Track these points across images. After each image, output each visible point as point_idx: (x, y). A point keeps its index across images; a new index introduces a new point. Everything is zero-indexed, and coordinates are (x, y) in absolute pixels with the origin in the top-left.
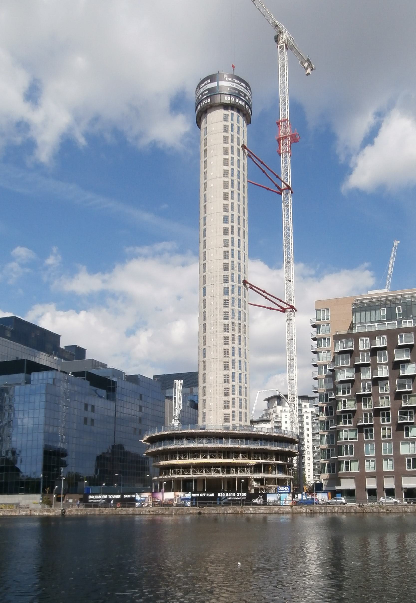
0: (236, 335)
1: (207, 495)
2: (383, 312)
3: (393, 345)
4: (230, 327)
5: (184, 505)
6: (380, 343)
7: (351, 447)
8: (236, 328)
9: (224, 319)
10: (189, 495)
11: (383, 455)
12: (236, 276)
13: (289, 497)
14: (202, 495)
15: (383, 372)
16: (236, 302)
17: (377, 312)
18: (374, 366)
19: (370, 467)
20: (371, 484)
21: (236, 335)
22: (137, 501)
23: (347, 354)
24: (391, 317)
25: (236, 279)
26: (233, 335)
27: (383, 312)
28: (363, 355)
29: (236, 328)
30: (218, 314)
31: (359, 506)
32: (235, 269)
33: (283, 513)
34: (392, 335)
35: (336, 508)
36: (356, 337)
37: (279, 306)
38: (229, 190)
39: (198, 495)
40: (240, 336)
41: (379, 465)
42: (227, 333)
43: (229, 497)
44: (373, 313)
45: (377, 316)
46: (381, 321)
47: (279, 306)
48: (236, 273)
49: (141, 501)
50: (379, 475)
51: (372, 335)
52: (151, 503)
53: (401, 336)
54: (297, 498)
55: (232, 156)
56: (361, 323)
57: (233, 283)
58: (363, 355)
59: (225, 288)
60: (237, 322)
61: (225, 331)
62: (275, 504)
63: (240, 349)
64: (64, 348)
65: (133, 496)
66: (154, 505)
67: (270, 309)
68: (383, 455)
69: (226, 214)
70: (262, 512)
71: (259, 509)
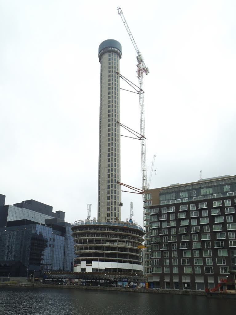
0: (113, 207)
1: (92, 280)
2: (174, 195)
3: (177, 212)
4: (110, 203)
5: (83, 285)
6: (172, 210)
7: (158, 261)
8: (113, 203)
9: (108, 200)
10: (84, 281)
11: (173, 265)
12: (114, 180)
13: (127, 284)
14: (90, 281)
15: (173, 224)
16: (113, 192)
17: (171, 195)
18: (168, 221)
19: (167, 270)
20: (167, 280)
21: (113, 207)
22: (64, 282)
23: (218, 209)
24: (178, 197)
25: (114, 181)
26: (112, 207)
27: (174, 195)
28: (192, 213)
29: (113, 203)
30: (105, 197)
31: (157, 290)
32: (113, 177)
33: (176, 294)
34: (177, 206)
35: (146, 290)
36: (160, 207)
37: (139, 192)
38: (111, 142)
39: (88, 280)
40: (115, 207)
41: (171, 270)
42: (109, 206)
43: (101, 282)
44: (169, 195)
45: (171, 196)
46: (173, 199)
47: (139, 192)
48: (114, 179)
49: (65, 282)
50: (171, 275)
51: (168, 206)
52: (69, 283)
53: (182, 207)
54: (131, 284)
55: (112, 127)
56: (163, 200)
57: (112, 183)
58: (227, 209)
59: (108, 185)
60: (113, 201)
61: (108, 205)
62: (121, 286)
63: (115, 213)
64: (55, 212)
65: (62, 280)
66: (70, 284)
67: (135, 193)
68: (173, 265)
69: (109, 152)
70: (113, 290)
71: (111, 288)
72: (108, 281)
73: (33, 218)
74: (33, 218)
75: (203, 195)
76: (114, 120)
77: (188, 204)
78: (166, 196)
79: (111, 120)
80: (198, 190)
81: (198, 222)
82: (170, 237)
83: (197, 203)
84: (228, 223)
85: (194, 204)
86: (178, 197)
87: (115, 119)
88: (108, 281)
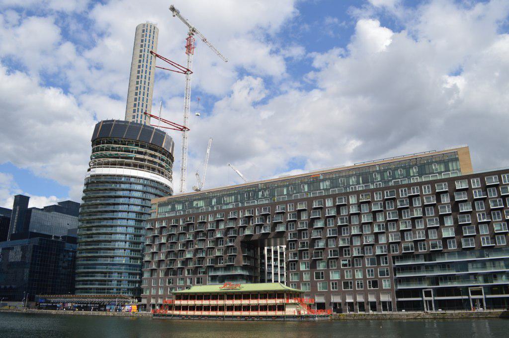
6: (445, 188)
49: (59, 307)
51: (161, 220)
72: (98, 305)
73: (68, 224)
74: (68, 224)
75: (322, 190)
76: (140, 110)
77: (286, 203)
78: (164, 208)
79: (137, 110)
80: (256, 193)
81: (437, 211)
82: (414, 233)
83: (296, 202)
84: (478, 212)
85: (477, 178)
86: (173, 209)
87: (142, 109)
88: (98, 305)
